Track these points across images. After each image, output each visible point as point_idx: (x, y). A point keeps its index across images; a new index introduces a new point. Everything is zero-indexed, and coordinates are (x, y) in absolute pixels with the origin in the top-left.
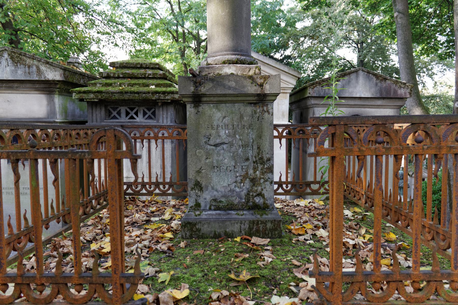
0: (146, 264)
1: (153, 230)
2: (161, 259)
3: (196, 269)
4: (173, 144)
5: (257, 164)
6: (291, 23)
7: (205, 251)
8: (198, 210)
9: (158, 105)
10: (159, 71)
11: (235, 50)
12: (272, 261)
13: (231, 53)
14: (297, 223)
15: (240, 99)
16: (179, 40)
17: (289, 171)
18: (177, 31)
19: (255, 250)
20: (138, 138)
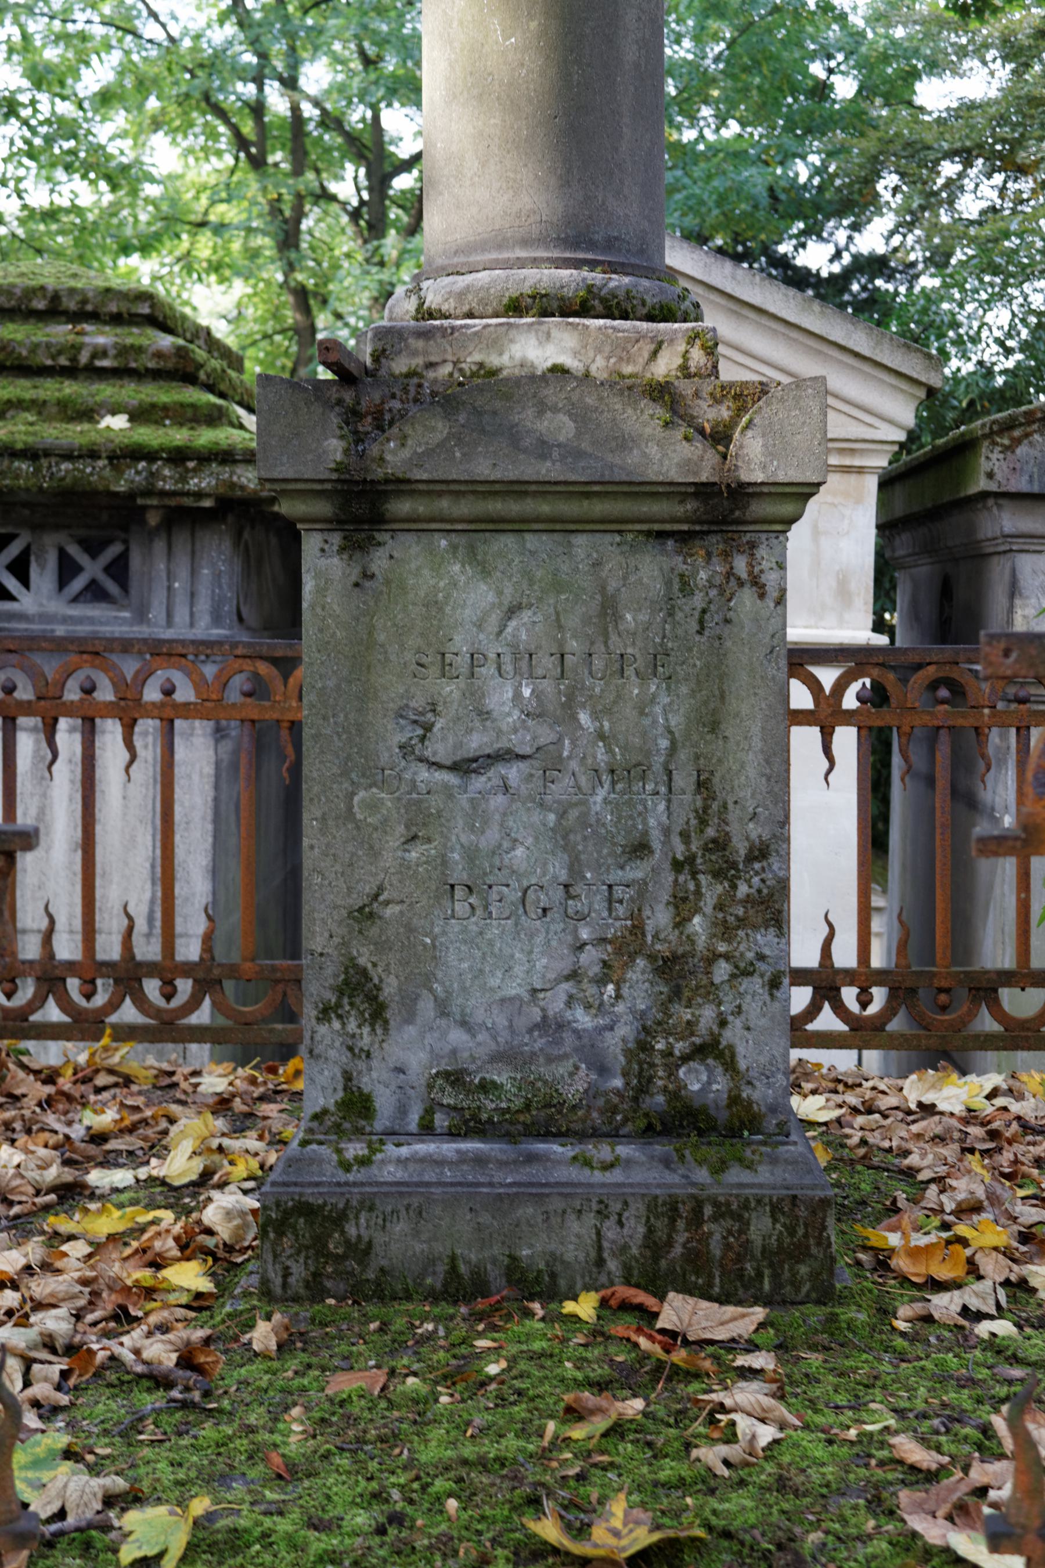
0: (51, 1454)
1: (98, 1248)
2: (137, 1424)
3: (338, 1485)
4: (227, 746)
5: (694, 874)
6: (890, 80)
7: (392, 1372)
8: (359, 1131)
9: (143, 522)
10: (151, 332)
11: (577, 236)
12: (776, 1442)
13: (556, 254)
14: (920, 1214)
15: (599, 508)
16: (271, 159)
17: (877, 901)
18: (258, 109)
19: (680, 1372)
20: (27, 709)
